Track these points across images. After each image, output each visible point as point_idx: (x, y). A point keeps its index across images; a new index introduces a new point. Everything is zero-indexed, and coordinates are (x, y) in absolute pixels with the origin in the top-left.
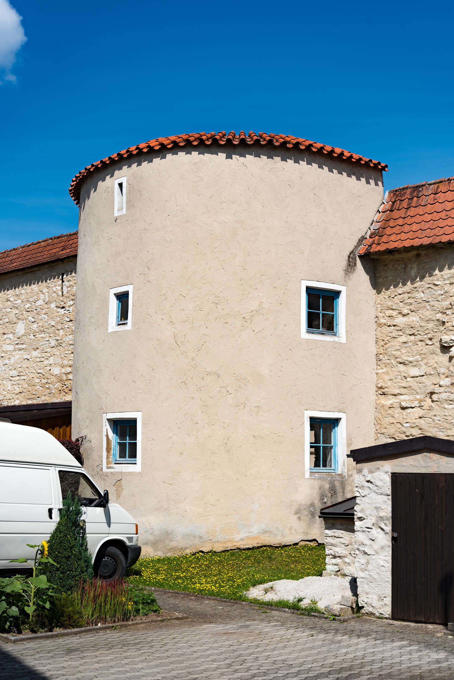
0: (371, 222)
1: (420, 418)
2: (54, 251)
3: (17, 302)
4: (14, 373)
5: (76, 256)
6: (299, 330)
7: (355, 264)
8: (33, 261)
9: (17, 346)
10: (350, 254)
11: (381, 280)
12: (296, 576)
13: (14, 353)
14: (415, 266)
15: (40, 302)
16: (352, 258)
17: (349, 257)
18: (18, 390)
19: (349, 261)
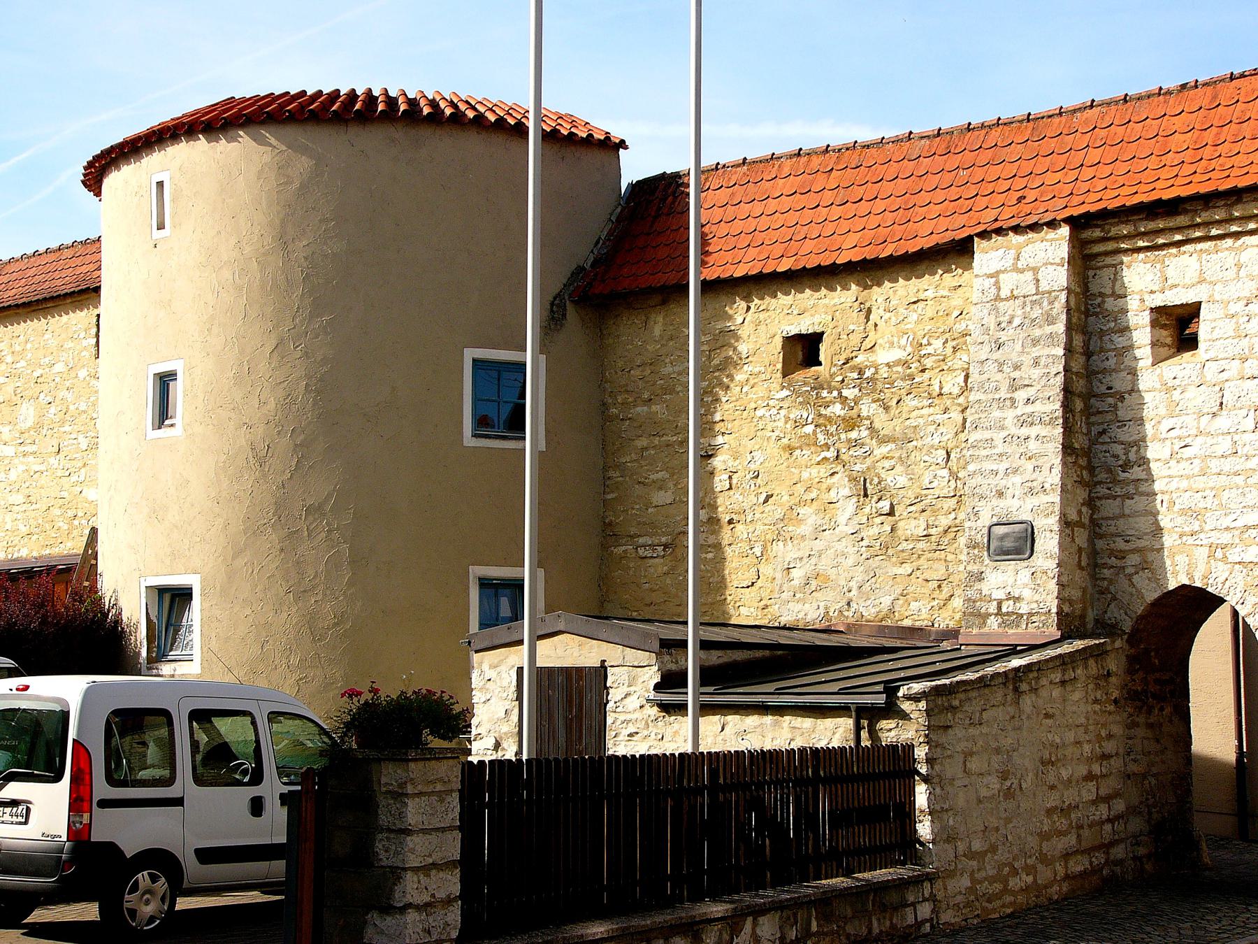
0: (149, 390)
1: (1221, 404)
2: (84, 269)
3: (18, 365)
4: (19, 498)
5: (97, 290)
6: (461, 433)
7: (564, 315)
8: (46, 289)
9: (22, 449)
10: (555, 298)
11: (611, 341)
12: (817, 756)
13: (16, 461)
14: (660, 319)
15: (59, 367)
16: (558, 306)
17: (552, 304)
18: (24, 530)
19: (552, 311)
